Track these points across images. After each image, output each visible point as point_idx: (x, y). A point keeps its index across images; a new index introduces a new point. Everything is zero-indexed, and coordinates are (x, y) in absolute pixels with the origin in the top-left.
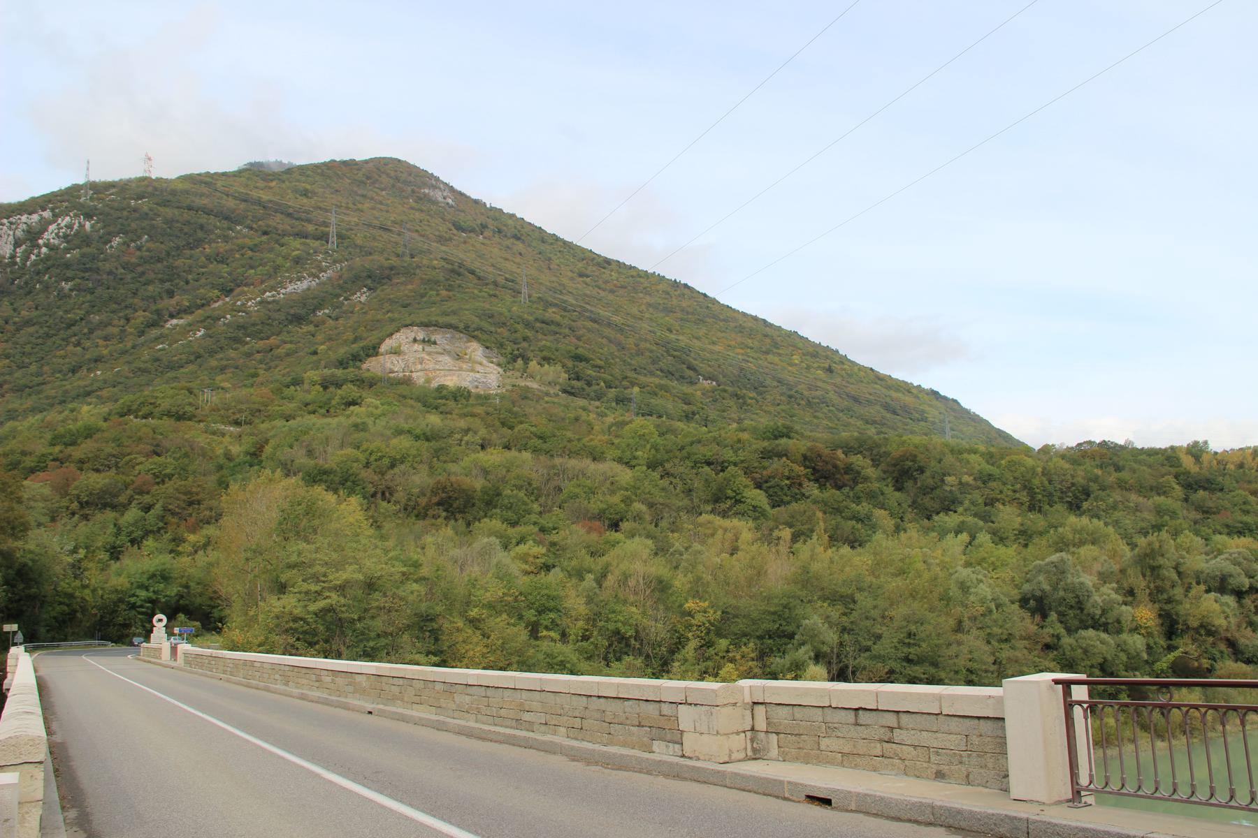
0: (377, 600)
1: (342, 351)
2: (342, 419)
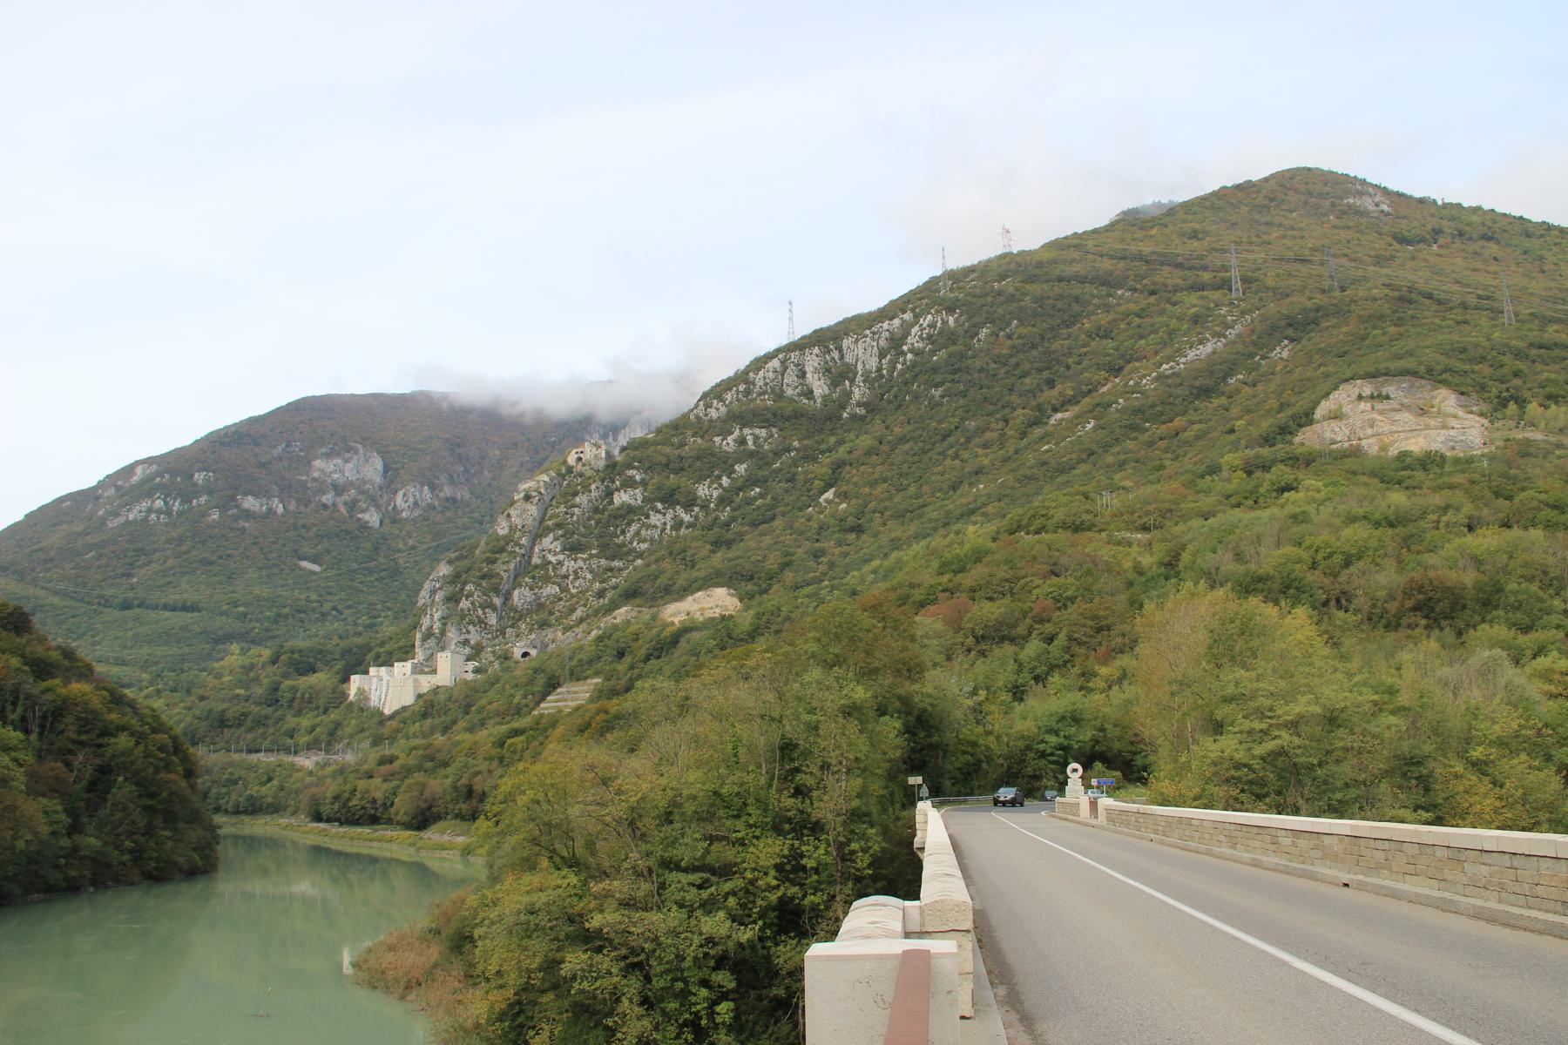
0: (1342, 738)
1: (1266, 425)
2: (1275, 510)
